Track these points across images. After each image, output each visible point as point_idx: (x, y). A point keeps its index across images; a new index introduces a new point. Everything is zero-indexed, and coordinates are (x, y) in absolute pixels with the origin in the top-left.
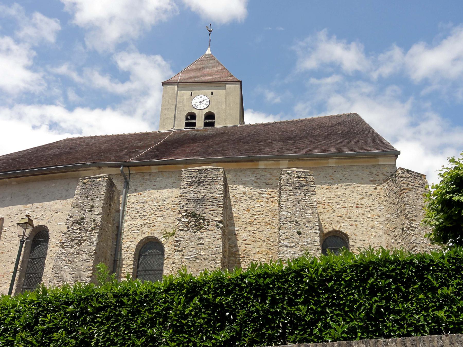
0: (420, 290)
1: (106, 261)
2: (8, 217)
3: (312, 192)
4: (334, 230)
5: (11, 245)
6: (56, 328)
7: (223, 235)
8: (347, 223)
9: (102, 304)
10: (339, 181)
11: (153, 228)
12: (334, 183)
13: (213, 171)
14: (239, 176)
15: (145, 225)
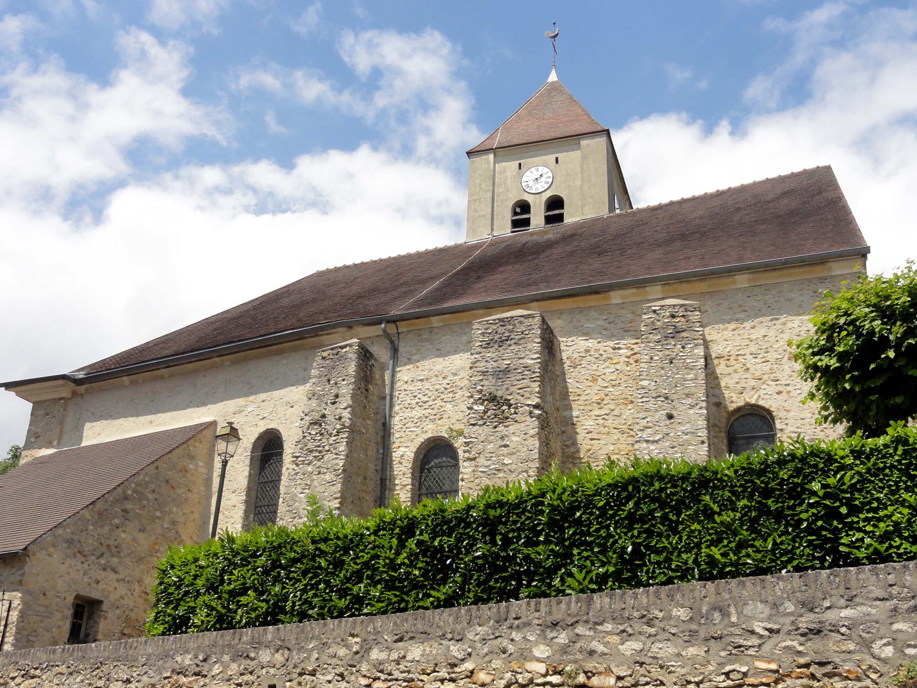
0: (694, 518)
1: (367, 481)
3: (696, 341)
4: (748, 405)
6: (244, 591)
7: (542, 428)
8: (772, 388)
9: (298, 553)
10: (756, 314)
11: (440, 422)
12: (748, 318)
13: (522, 319)
14: (579, 321)
15: (426, 417)
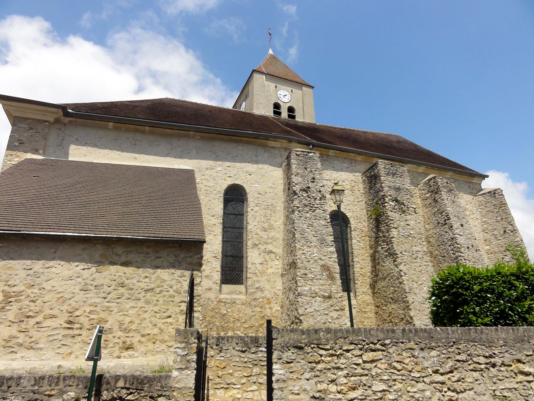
2: (198, 170)
5: (207, 199)
